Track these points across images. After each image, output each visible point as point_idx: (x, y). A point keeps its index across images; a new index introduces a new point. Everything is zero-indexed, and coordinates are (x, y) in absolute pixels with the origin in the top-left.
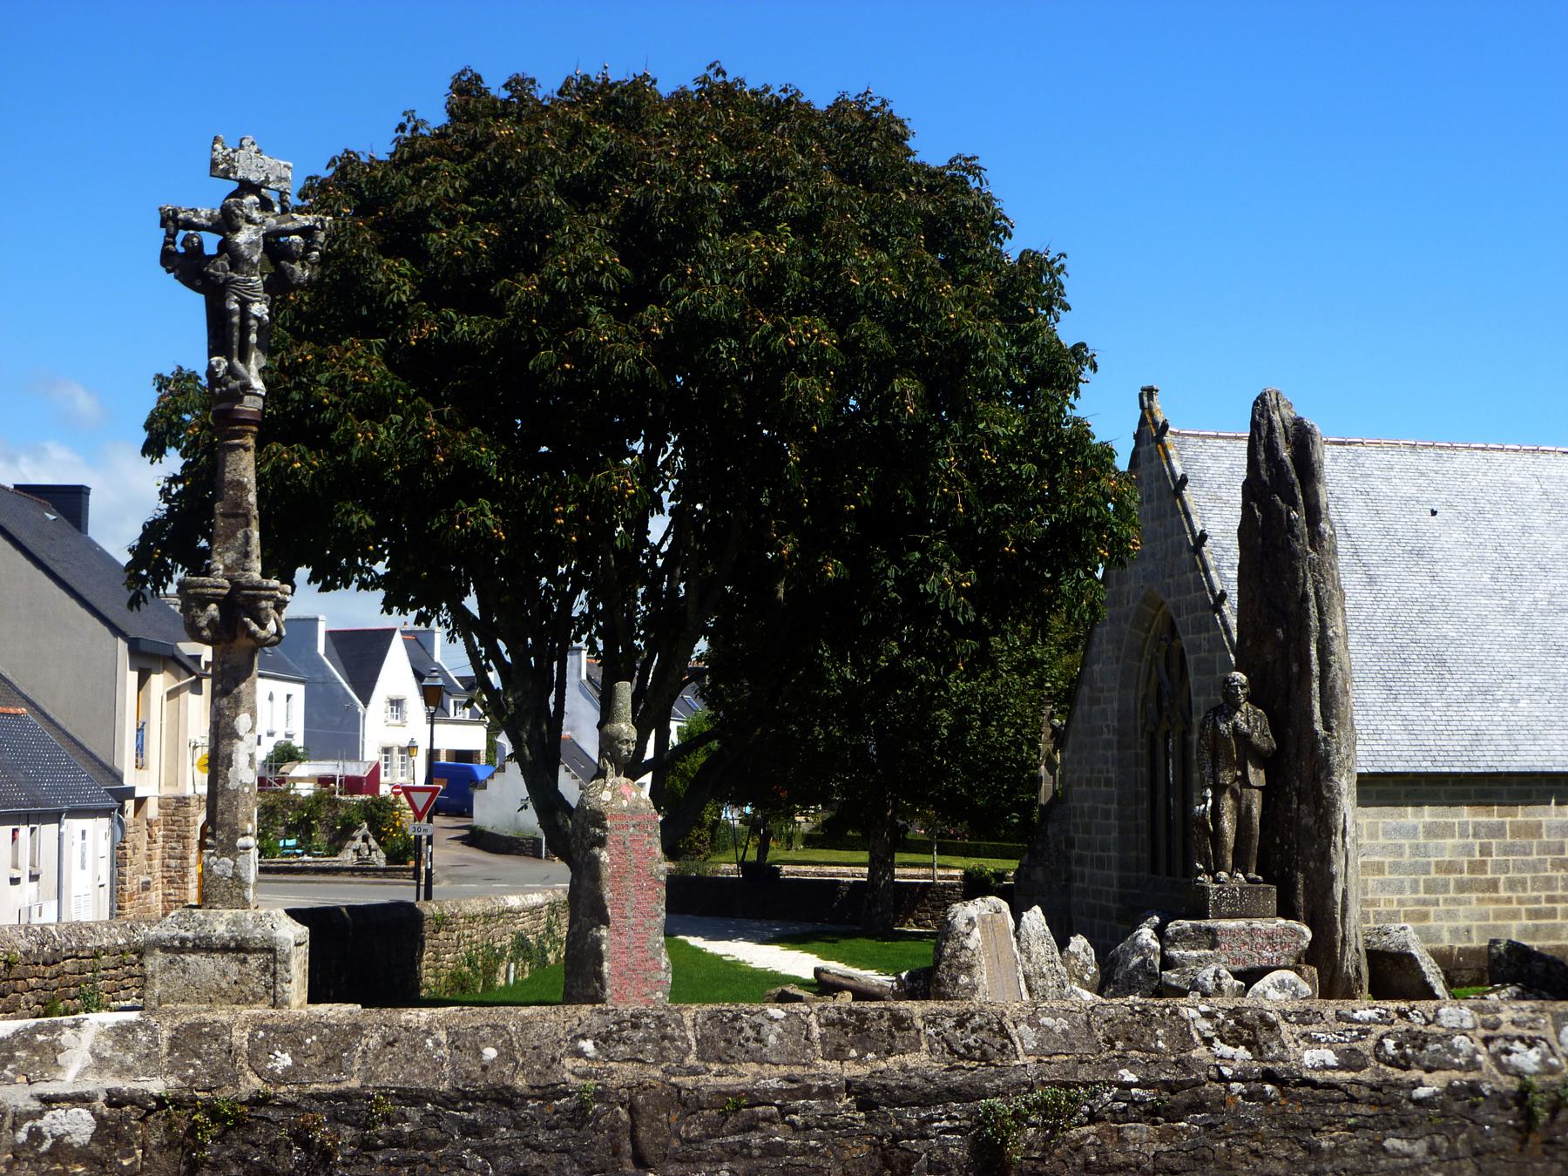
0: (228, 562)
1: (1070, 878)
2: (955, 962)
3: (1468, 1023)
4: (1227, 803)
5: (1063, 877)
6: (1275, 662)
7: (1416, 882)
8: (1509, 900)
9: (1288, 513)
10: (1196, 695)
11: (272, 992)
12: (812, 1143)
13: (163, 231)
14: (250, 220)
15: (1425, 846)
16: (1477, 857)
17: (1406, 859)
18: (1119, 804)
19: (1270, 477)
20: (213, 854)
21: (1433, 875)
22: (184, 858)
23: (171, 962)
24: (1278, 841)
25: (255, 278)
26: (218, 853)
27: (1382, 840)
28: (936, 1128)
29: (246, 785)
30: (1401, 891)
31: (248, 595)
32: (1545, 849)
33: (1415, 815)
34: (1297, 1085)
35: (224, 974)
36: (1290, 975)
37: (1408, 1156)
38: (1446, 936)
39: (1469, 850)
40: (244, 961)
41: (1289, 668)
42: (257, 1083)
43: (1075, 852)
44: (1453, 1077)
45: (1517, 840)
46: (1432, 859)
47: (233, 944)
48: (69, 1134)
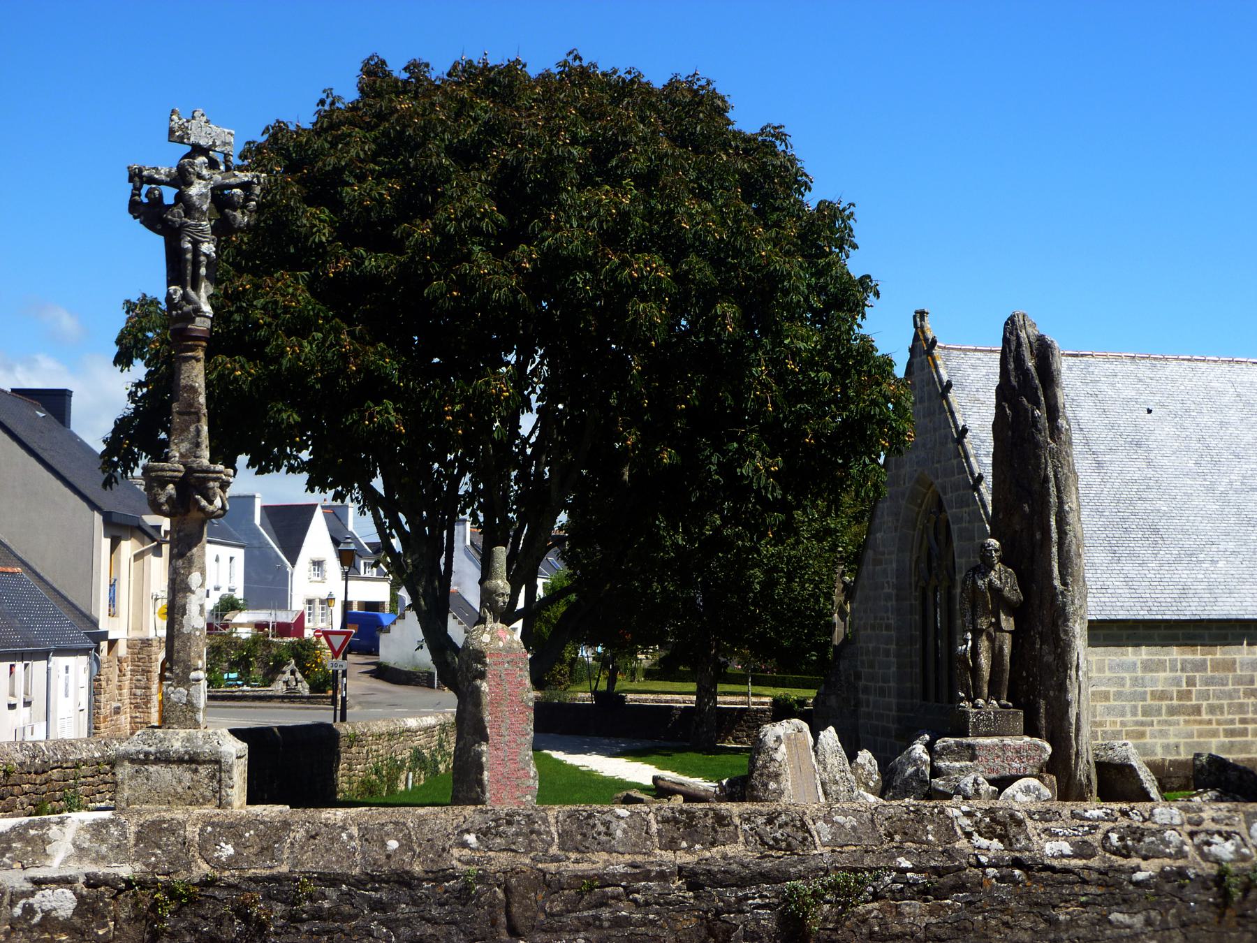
0: (183, 450)
2: (766, 771)
3: (1177, 821)
4: (984, 644)
6: (1022, 531)
7: (1135, 707)
8: (1210, 722)
9: (1033, 411)
10: (959, 557)
11: (218, 795)
12: (651, 916)
13: (131, 185)
14: (200, 177)
15: (1142, 678)
16: (1184, 687)
17: (1127, 689)
18: (897, 644)
19: (1018, 382)
20: (171, 685)
21: (1149, 702)
22: (147, 688)
23: (137, 771)
24: (1024, 674)
25: (204, 223)
26: (175, 684)
27: (1108, 674)
28: (751, 905)
29: (197, 629)
30: (1123, 714)
31: (198, 477)
32: (1239, 681)
33: (1135, 654)
34: (1040, 870)
35: (180, 781)
36: (1034, 782)
37: (1129, 927)
38: (1159, 750)
39: (1177, 682)
40: (196, 771)
41: (1033, 536)
42: (206, 868)
44: (1165, 863)
45: (1216, 674)
46: (1148, 689)
47: (186, 757)
48: (55, 909)
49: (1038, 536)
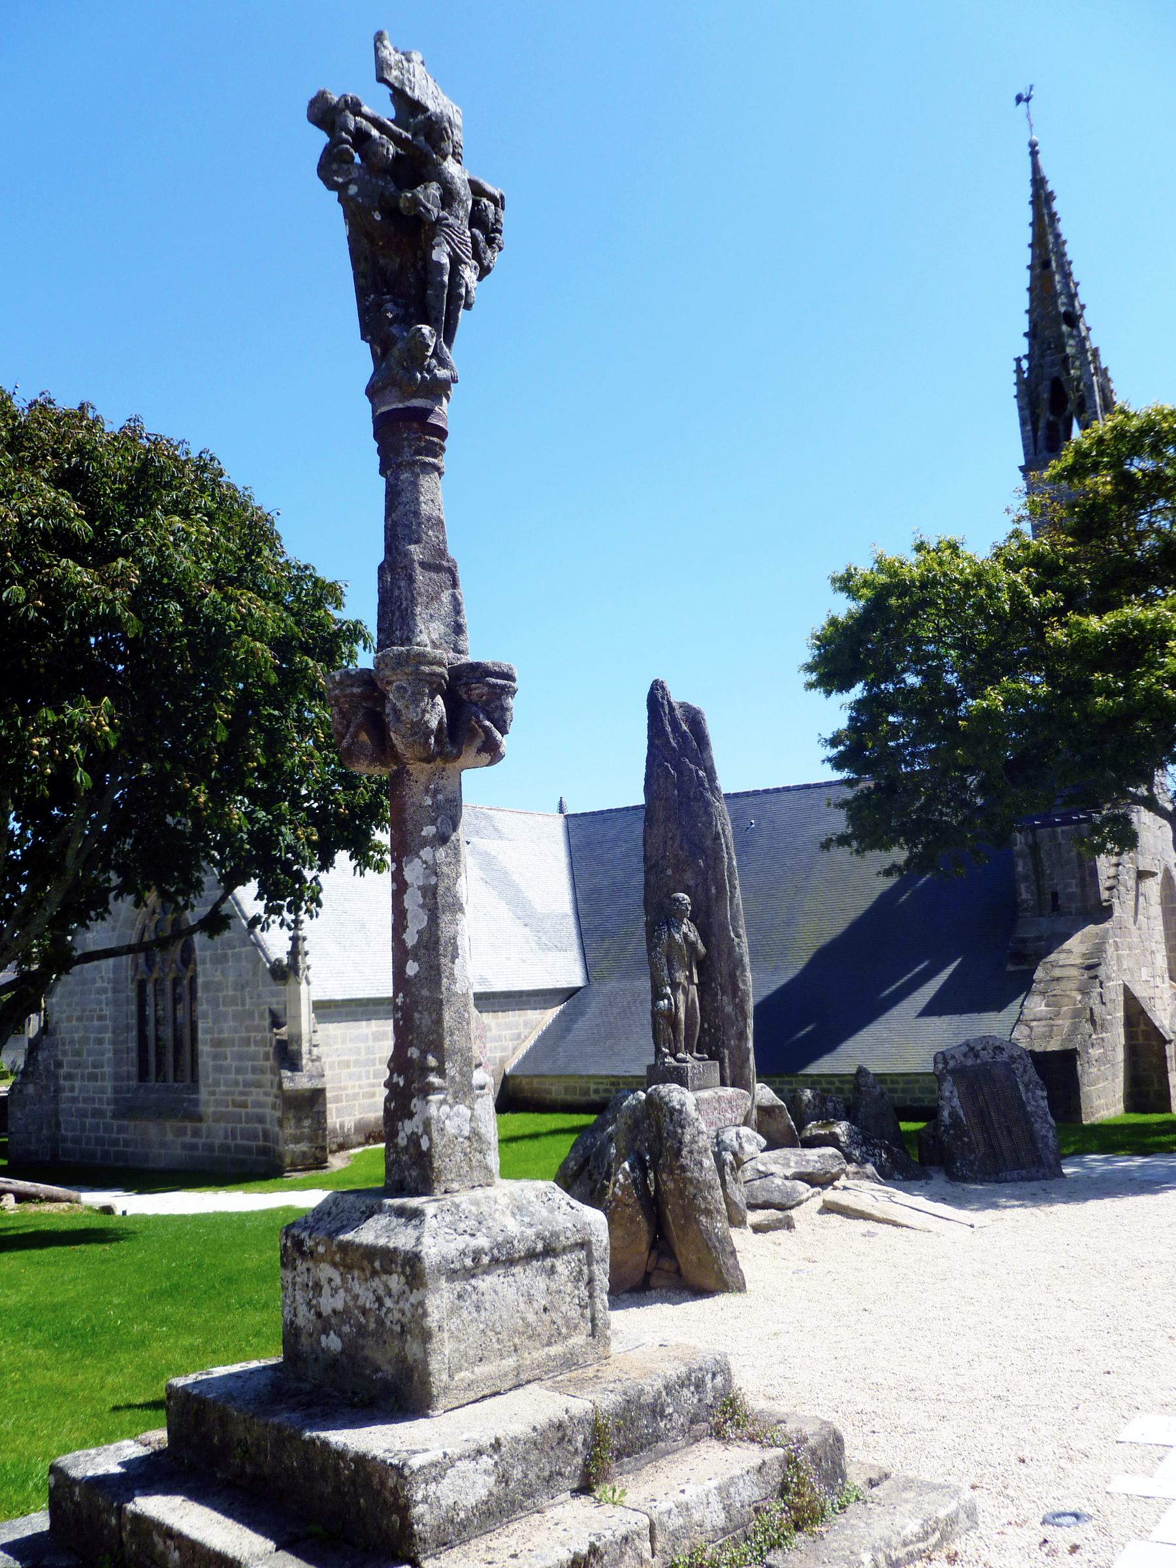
1: (58, 1090)
2: (695, 1147)
4: (681, 997)
5: (52, 1089)
6: (697, 886)
7: (368, 1072)
9: (697, 772)
10: (202, 950)
11: (588, 1312)
17: (363, 1057)
18: (114, 1032)
19: (678, 743)
23: (460, 1297)
27: (349, 1045)
30: (360, 1078)
31: (495, 686)
33: (367, 1027)
35: (530, 1300)
40: (552, 1271)
41: (708, 890)
43: (64, 1071)
46: (377, 1056)
47: (540, 1246)
49: (713, 891)
